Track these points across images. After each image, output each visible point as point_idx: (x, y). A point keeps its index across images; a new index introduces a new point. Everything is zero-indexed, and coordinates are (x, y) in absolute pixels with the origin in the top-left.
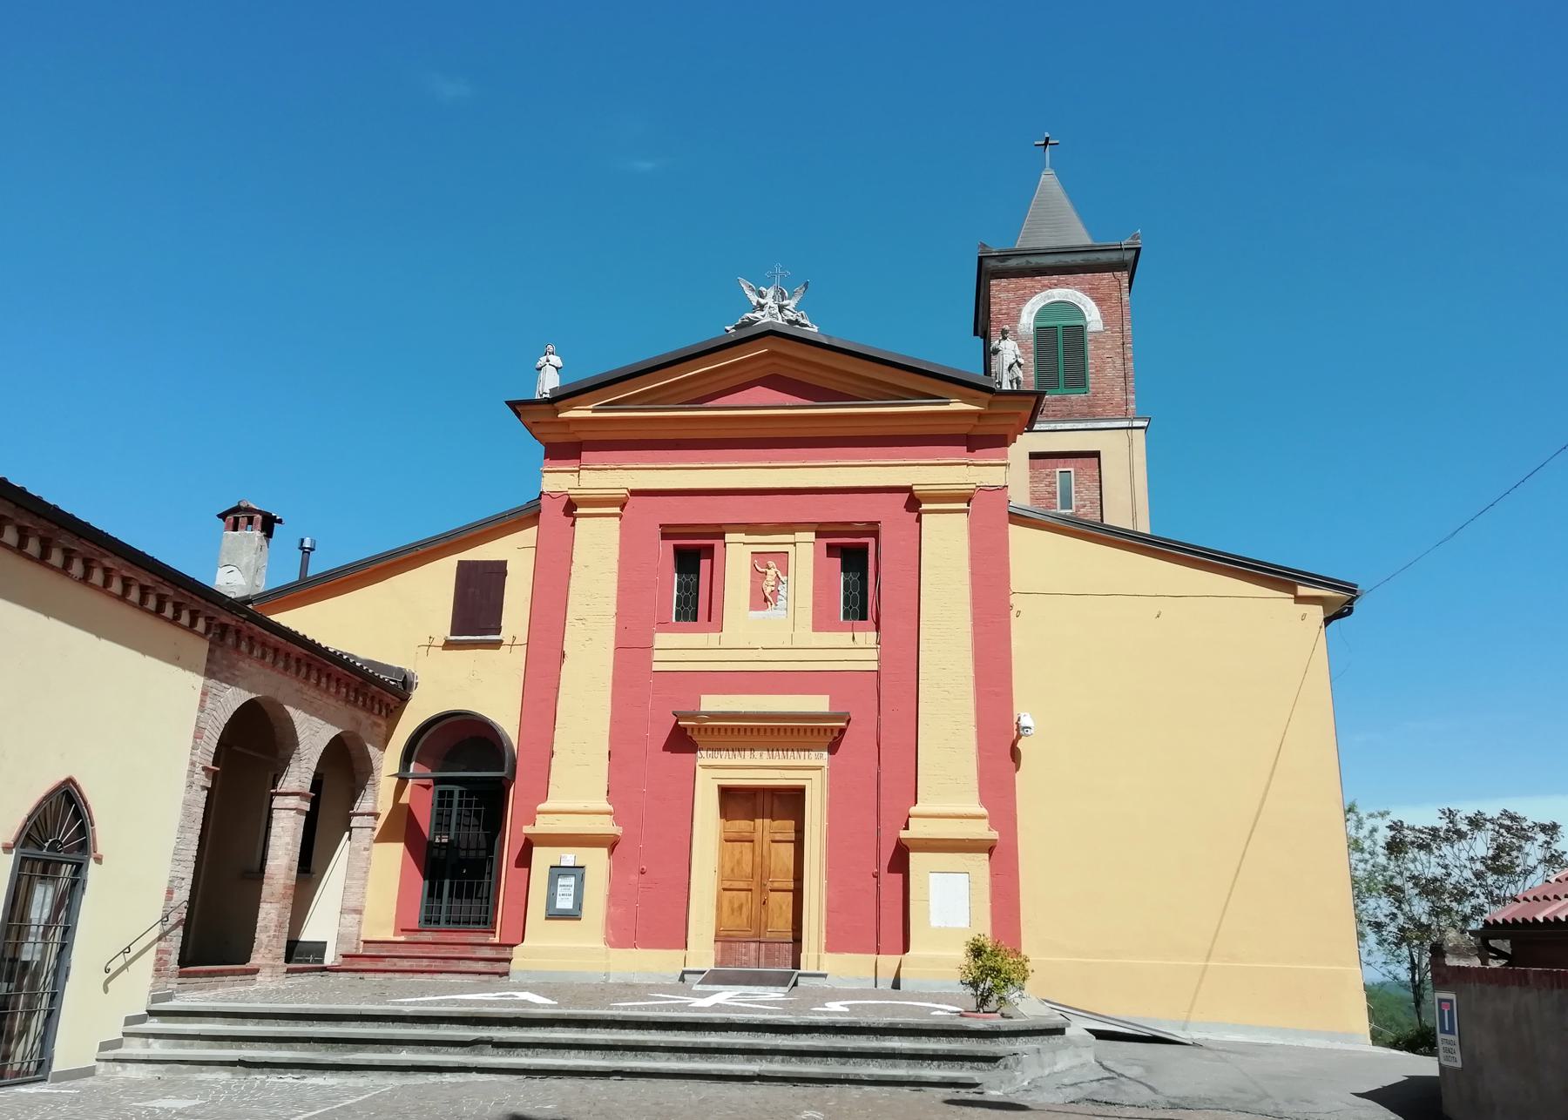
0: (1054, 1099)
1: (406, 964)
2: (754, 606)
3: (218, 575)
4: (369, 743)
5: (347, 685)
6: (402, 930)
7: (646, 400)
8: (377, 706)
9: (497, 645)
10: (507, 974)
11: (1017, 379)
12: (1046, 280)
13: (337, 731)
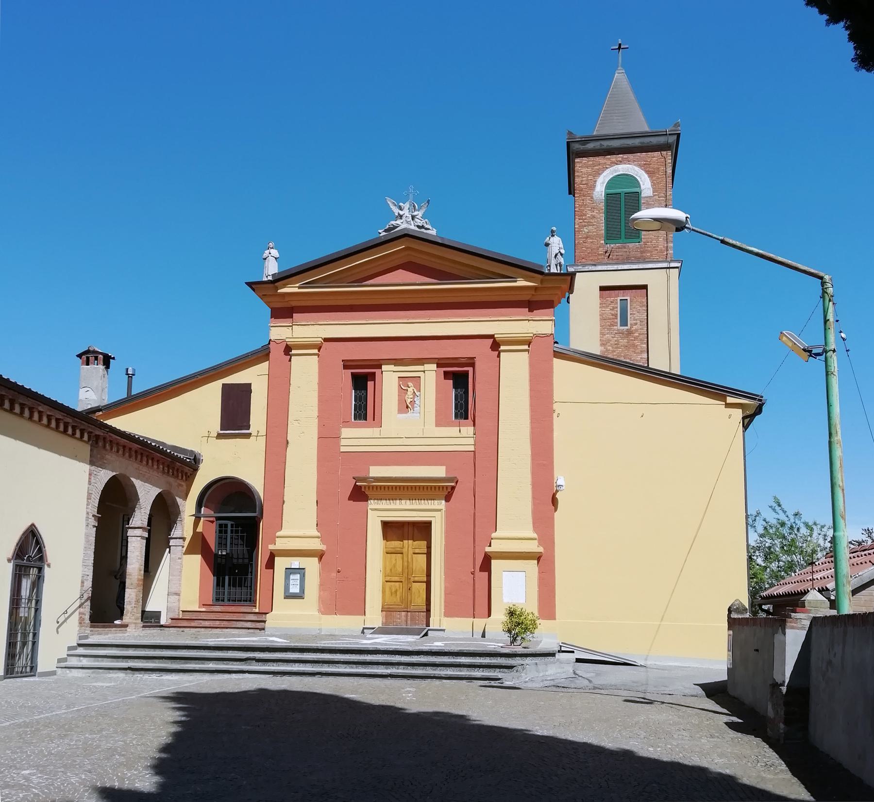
0: (537, 686)
1: (207, 624)
2: (400, 411)
3: (80, 394)
4: (177, 496)
5: (163, 464)
6: (203, 605)
7: (328, 281)
8: (180, 474)
9: (248, 436)
10: (263, 629)
11: (560, 263)
12: (613, 158)
13: (160, 491)
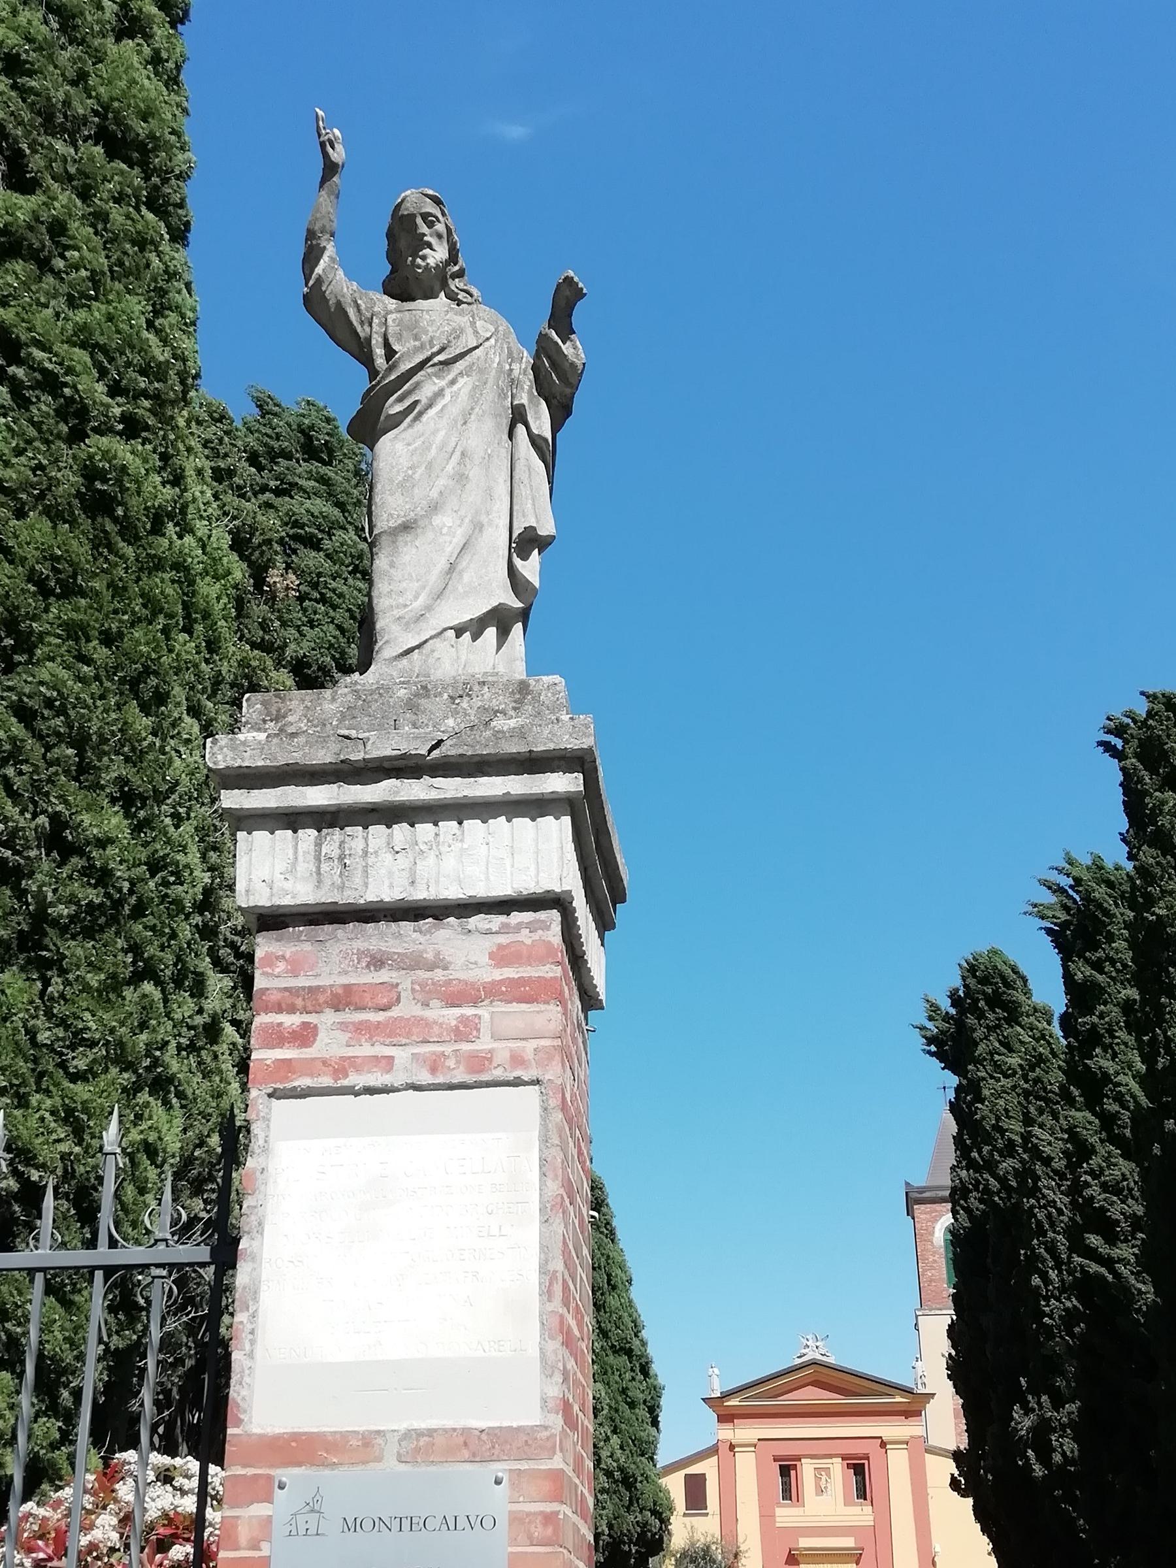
2: (817, 1494)
9: (707, 1514)
